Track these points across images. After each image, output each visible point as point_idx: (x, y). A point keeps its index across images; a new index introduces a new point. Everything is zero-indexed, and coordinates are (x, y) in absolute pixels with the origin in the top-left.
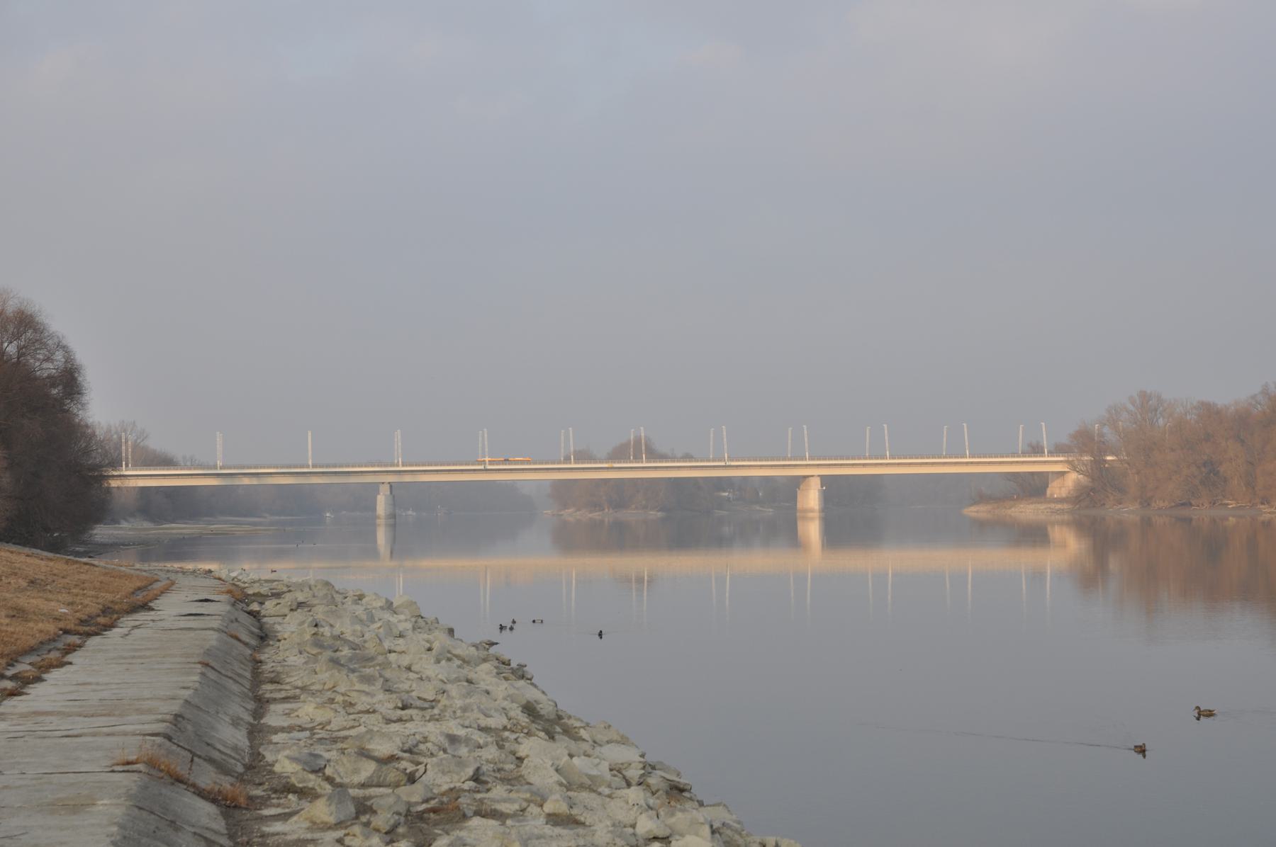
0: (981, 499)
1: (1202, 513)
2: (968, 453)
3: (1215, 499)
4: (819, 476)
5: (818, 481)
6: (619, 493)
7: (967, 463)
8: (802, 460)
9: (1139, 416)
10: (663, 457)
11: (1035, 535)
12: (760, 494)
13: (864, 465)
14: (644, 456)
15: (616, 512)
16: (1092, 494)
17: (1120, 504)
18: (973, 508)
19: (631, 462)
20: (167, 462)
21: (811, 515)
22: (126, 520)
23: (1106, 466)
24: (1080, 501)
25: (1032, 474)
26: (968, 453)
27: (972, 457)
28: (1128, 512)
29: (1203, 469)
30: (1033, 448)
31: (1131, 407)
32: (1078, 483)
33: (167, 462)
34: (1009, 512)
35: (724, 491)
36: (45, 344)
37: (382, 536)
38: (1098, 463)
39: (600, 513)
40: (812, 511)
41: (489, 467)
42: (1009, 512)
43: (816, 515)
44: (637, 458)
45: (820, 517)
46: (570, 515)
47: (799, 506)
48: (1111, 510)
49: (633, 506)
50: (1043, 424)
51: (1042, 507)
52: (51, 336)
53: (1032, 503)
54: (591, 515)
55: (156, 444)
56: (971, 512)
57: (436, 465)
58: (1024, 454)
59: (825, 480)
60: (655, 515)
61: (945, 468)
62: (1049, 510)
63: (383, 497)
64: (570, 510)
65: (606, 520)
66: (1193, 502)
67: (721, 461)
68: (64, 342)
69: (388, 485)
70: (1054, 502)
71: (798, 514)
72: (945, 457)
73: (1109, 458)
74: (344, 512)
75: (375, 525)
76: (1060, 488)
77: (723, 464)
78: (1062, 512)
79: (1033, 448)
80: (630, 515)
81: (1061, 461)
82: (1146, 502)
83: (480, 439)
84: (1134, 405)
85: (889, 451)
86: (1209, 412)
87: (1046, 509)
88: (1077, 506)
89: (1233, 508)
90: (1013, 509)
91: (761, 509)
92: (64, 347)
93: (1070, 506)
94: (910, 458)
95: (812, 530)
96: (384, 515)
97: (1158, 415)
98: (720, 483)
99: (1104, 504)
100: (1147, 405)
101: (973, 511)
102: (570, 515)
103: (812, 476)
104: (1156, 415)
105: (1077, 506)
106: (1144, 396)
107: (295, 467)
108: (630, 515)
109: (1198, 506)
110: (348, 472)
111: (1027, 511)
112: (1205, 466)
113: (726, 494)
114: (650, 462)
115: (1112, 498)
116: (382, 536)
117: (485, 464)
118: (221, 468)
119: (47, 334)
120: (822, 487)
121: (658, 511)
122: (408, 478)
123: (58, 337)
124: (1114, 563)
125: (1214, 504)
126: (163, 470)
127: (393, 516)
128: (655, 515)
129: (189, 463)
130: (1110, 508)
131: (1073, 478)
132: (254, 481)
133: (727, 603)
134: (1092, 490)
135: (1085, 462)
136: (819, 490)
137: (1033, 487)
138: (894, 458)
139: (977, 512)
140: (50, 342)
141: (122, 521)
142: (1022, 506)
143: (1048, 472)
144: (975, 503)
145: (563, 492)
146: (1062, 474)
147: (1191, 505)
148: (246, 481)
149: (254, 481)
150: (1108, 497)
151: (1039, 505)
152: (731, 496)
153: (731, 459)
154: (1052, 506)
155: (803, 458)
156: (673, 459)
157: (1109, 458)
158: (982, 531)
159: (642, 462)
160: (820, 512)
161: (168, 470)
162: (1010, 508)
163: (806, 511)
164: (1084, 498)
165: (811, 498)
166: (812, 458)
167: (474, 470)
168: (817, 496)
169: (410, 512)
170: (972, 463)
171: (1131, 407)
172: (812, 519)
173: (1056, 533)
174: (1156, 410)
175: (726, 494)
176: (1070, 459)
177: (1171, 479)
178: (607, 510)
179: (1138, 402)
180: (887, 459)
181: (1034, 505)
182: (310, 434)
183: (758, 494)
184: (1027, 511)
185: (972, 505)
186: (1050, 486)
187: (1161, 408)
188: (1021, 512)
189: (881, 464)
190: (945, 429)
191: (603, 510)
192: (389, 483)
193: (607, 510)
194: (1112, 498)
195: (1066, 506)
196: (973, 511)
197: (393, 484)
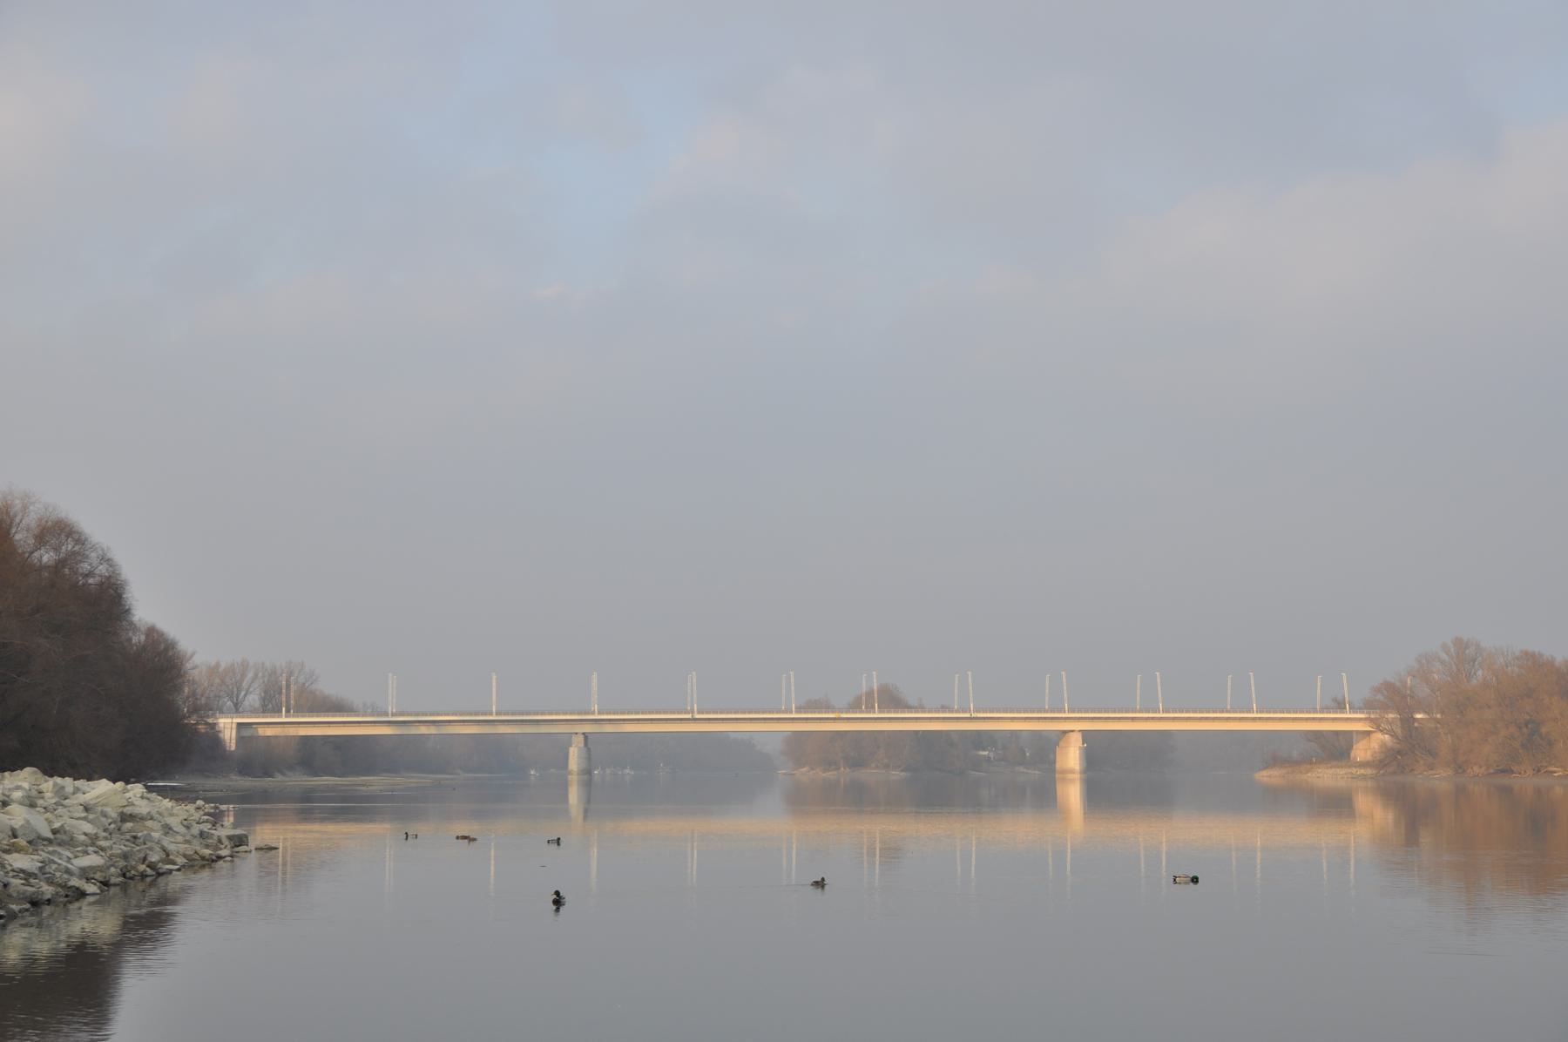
0: (1275, 761)
1: (1525, 781)
2: (1255, 708)
3: (1539, 765)
4: (1080, 731)
5: (581, 738)
6: (857, 749)
7: (1254, 719)
8: (1248, 712)
9: (1454, 667)
10: (909, 708)
11: (1337, 805)
12: (1028, 754)
13: (1133, 719)
14: (284, 709)
15: (853, 771)
16: (1399, 757)
17: (1432, 769)
18: (1265, 773)
19: (861, 712)
20: (338, 707)
21: (1070, 776)
22: (283, 774)
23: (1416, 725)
24: (1385, 765)
25: (1337, 733)
26: (1255, 708)
27: (1354, 713)
28: (1436, 779)
29: (1525, 730)
30: (1339, 703)
31: (1445, 657)
32: (1383, 745)
33: (338, 707)
34: (1304, 777)
35: (984, 750)
36: (87, 557)
37: (574, 796)
38: (1407, 721)
39: (835, 773)
40: (1072, 771)
41: (697, 716)
42: (1304, 777)
43: (1077, 776)
44: (870, 708)
45: (1081, 779)
46: (805, 774)
47: (1058, 766)
48: (1420, 776)
49: (873, 765)
50: (1158, 673)
51: (1342, 772)
52: (94, 548)
53: (1331, 768)
54: (824, 775)
55: (328, 687)
56: (1263, 776)
57: (650, 713)
58: (1325, 709)
59: (1086, 735)
60: (897, 775)
61: (1201, 724)
62: (1350, 776)
63: (576, 749)
64: (805, 769)
65: (842, 781)
66: (1514, 769)
67: (966, 712)
68: (109, 555)
69: (583, 736)
70: (1355, 767)
71: (1057, 776)
72: (957, 712)
73: (1419, 716)
74: (553, 770)
75: (565, 786)
76: (1366, 750)
77: (968, 715)
78: (1364, 777)
79: (1339, 703)
80: (869, 775)
81: (1360, 719)
82: (1460, 768)
83: (689, 684)
84: (1447, 654)
85: (496, 706)
86: (1534, 663)
87: (1346, 774)
88: (1382, 772)
89: (1559, 776)
90: (1309, 774)
91: (1025, 770)
92: (108, 560)
93: (1374, 772)
94: (1294, 712)
95: (1073, 794)
96: (576, 770)
97: (1477, 667)
98: (980, 739)
99: (1412, 770)
100: (1464, 654)
101: (1267, 776)
102: (805, 774)
103: (1073, 731)
104: (1473, 666)
105: (1382, 772)
106: (1459, 642)
107: (529, 713)
108: (869, 775)
109: (1520, 774)
110: (538, 721)
111: (1326, 777)
112: (1527, 726)
113: (986, 753)
114: (884, 712)
115: (1422, 762)
116: (574, 796)
117: (693, 712)
118: (393, 715)
119: (89, 546)
120: (1083, 744)
121: (902, 771)
122: (608, 728)
123: (103, 550)
124: (1426, 838)
125: (1539, 771)
126: (328, 716)
127: (587, 772)
128: (897, 775)
129: (369, 711)
130: (1420, 774)
131: (1380, 739)
132: (433, 730)
133: (492, 880)
134: (1399, 752)
135: (1390, 720)
136: (1080, 747)
137: (1335, 748)
138: (1074, 712)
139: (1270, 776)
140: (93, 555)
141: (277, 774)
142: (1320, 770)
143: (1351, 732)
144: (1267, 766)
145: (798, 744)
146: (1368, 733)
147: (1512, 772)
148: (423, 730)
149: (433, 730)
150: (1418, 762)
151: (1338, 770)
152: (992, 755)
153: (977, 711)
154: (1354, 770)
155: (1061, 710)
156: (922, 708)
157: (1419, 716)
158: (1276, 800)
159: (875, 712)
160: (1081, 773)
161: (318, 716)
162: (1307, 772)
163: (1065, 772)
164: (1394, 761)
165: (1071, 757)
166: (1072, 710)
167: (709, 719)
168: (1077, 755)
169: (627, 771)
170: (1260, 719)
171: (1445, 657)
172: (1072, 781)
173: (1363, 802)
174: (1475, 660)
175: (986, 753)
176: (1372, 716)
177: (1487, 740)
178: (842, 769)
179: (1452, 650)
180: (1065, 712)
181: (1333, 770)
182: (595, 676)
183: (1025, 754)
184: (1326, 777)
185: (1265, 768)
186: (1354, 747)
187: (1480, 658)
188: (1318, 777)
189: (1153, 718)
190: (1047, 679)
191: (839, 768)
192: (583, 734)
193: (842, 769)
194: (1422, 762)
195: (1369, 771)
196: (1267, 776)
197: (589, 735)
